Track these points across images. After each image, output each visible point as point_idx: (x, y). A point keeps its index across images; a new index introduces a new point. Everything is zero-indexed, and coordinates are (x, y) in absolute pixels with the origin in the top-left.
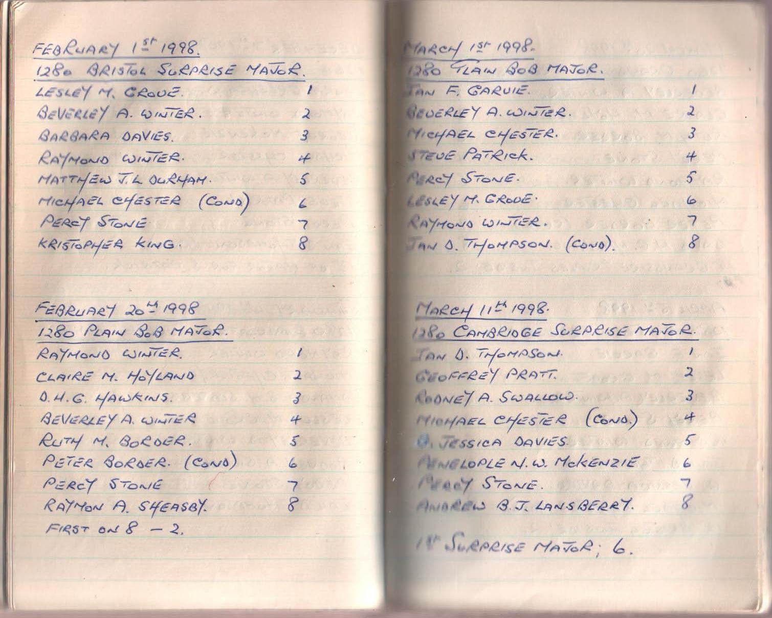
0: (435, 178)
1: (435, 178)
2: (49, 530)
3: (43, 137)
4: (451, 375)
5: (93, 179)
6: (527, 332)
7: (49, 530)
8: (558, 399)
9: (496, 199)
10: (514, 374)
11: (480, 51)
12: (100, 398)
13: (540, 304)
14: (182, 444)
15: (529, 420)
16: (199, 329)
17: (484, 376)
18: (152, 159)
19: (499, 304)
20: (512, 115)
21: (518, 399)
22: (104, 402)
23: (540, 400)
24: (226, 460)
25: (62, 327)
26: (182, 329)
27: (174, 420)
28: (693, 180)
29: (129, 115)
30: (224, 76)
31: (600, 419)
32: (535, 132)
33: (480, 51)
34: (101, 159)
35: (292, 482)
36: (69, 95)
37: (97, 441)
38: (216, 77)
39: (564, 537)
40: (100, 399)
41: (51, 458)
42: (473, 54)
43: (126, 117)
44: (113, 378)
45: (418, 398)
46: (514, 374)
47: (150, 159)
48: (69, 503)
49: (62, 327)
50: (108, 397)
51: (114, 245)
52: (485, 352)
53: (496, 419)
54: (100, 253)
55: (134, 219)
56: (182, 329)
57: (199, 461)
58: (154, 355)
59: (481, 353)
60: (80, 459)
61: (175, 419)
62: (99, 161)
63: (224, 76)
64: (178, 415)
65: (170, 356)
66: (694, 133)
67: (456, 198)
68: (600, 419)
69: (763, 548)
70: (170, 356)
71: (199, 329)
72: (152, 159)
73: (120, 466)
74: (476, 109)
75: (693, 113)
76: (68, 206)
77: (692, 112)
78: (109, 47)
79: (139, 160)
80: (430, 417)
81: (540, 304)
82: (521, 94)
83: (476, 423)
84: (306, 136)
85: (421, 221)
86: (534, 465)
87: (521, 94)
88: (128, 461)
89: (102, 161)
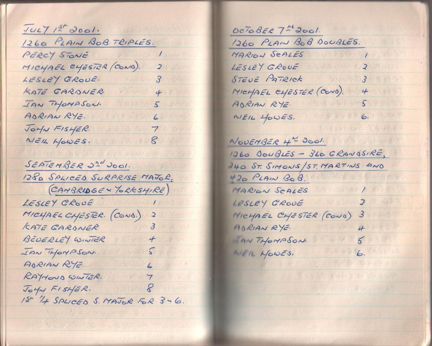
0: (43, 55)
1: (43, 55)
2: (52, 289)
4: (56, 127)
5: (76, 289)
7: (52, 289)
9: (76, 302)
10: (62, 302)
12: (42, 215)
14: (61, 217)
15: (287, 252)
16: (157, 176)
19: (289, 26)
22: (73, 292)
24: (133, 214)
26: (148, 190)
27: (37, 202)
32: (307, 214)
34: (131, 215)
35: (280, 28)
41: (267, 41)
43: (237, 106)
45: (235, 227)
46: (62, 302)
47: (83, 277)
49: (38, 174)
50: (256, 215)
51: (269, 31)
56: (148, 190)
59: (29, 103)
61: (307, 215)
62: (130, 216)
64: (44, 89)
66: (312, 42)
69: (428, 320)
71: (157, 176)
73: (290, 205)
75: (366, 68)
77: (366, 67)
80: (240, 213)
83: (267, 217)
84: (365, 80)
85: (253, 227)
88: (248, 226)
89: (131, 216)
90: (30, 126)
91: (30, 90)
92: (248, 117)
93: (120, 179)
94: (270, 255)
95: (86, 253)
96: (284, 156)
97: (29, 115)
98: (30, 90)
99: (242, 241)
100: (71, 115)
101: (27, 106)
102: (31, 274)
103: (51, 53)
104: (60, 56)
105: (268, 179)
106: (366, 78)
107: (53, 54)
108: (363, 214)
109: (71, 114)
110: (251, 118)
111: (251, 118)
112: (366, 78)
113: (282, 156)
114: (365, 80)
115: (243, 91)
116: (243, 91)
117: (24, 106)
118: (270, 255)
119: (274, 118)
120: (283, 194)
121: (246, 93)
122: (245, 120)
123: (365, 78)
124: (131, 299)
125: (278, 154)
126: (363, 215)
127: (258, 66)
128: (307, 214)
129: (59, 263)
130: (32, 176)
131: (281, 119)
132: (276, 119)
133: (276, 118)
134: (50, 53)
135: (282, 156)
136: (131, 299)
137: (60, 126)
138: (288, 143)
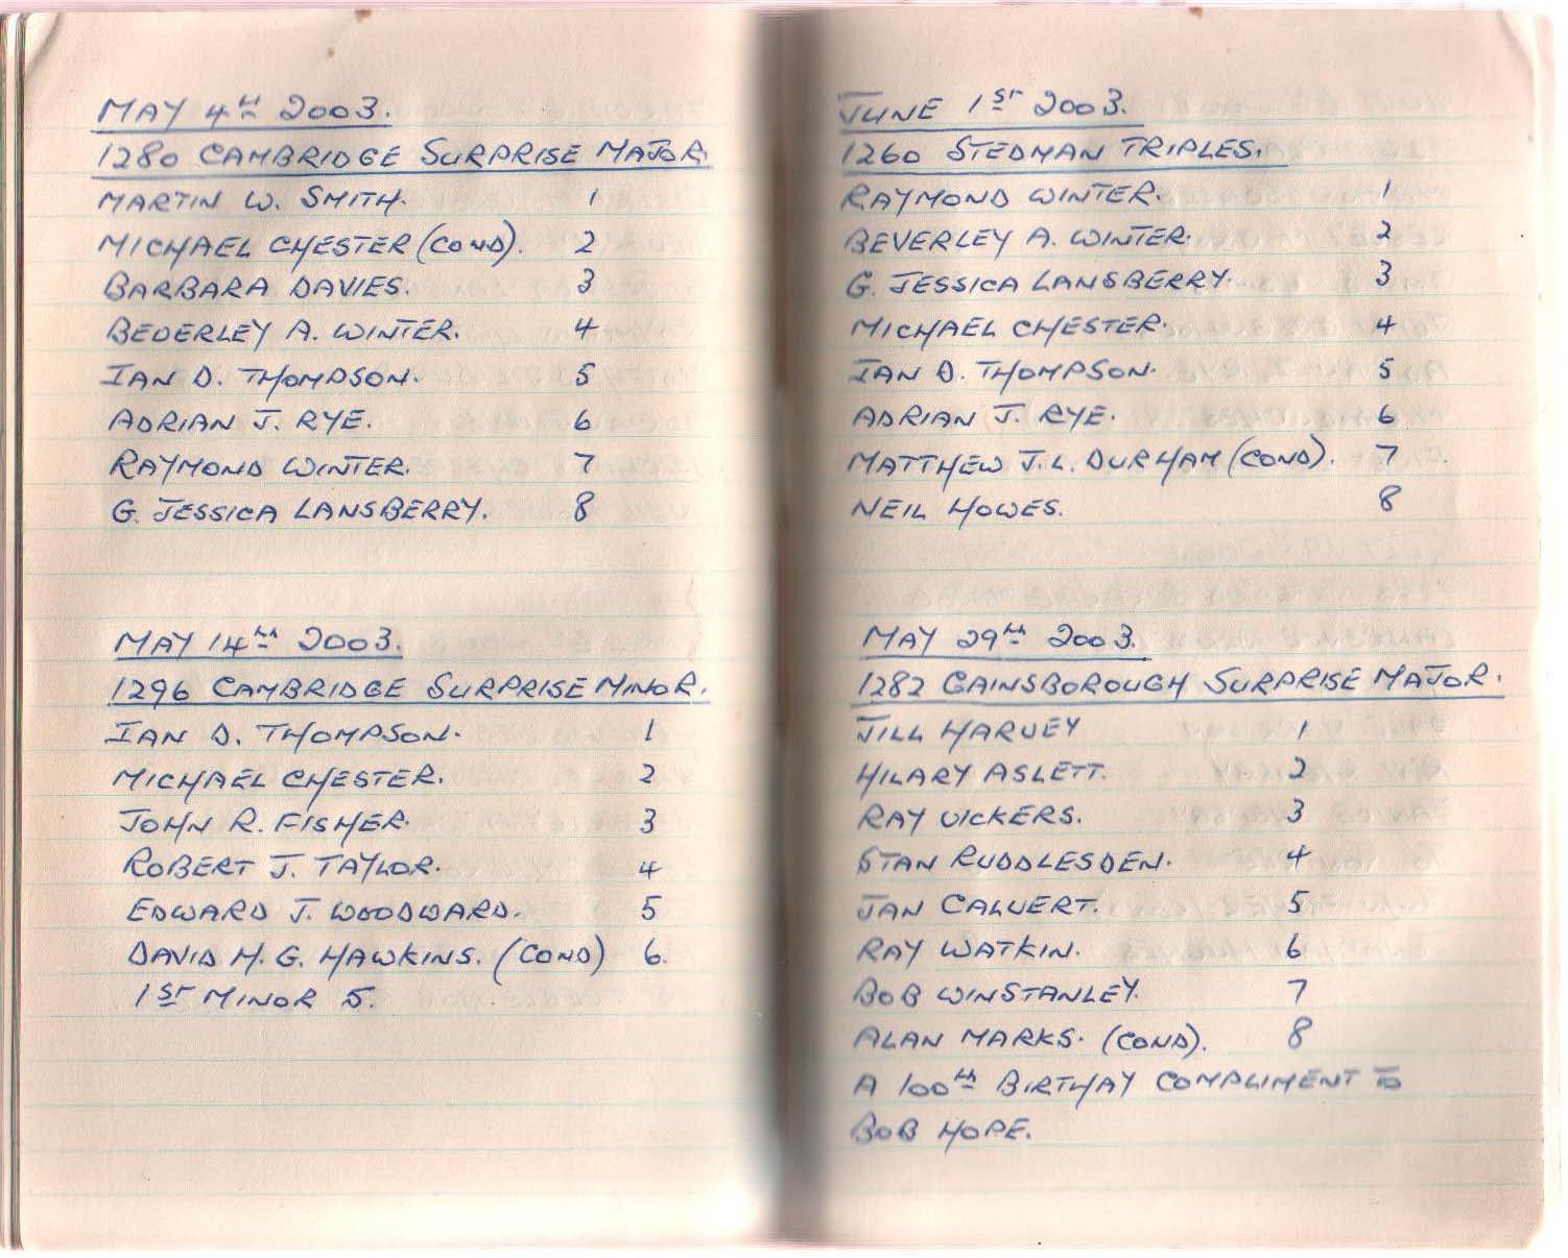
3: (114, 289)
6: (375, 689)
8: (439, 161)
11: (998, 109)
13: (581, 495)
17: (1037, 906)
18: (1135, 240)
20: (256, 208)
21: (954, 999)
23: (306, 517)
25: (157, 146)
28: (1012, 332)
29: (311, 335)
30: (559, 165)
31: (1131, 1040)
33: (998, 109)
36: (900, 739)
37: (969, 1035)
38: (1108, 120)
39: (164, 884)
40: (187, 784)
42: (986, 115)
44: (259, 958)
48: (927, 634)
52: (993, 369)
53: (288, 776)
54: (184, 838)
55: (206, 790)
57: (297, 777)
58: (1061, 199)
60: (342, 773)
63: (559, 165)
65: (413, 783)
67: (1007, 237)
68: (1131, 1040)
70: (413, 783)
72: (1135, 240)
74: (1131, 984)
76: (1164, 467)
78: (162, 108)
79: (1139, 240)
81: (581, 495)
82: (994, 157)
86: (333, 917)
87: (994, 157)
90: (268, 414)
91: (1004, 814)
92: (902, 507)
93: (234, 916)
94: (1025, 374)
95: (1034, 374)
96: (1002, 859)
97: (980, 682)
98: (1004, 814)
99: (877, 375)
100: (458, 508)
101: (115, 383)
102: (1242, 460)
103: (171, 103)
104: (297, 949)
105: (923, 777)
106: (1388, 270)
107: (932, 635)
108: (650, 821)
109: (457, 505)
110: (911, 512)
111: (911, 512)
112: (1388, 270)
113: (865, 119)
114: (1386, 274)
115: (971, 814)
116: (971, 814)
117: (106, 383)
118: (1025, 374)
119: (998, 513)
120: (946, 786)
121: (296, 782)
122: (1090, 1002)
123: (1386, 267)
124: (398, 458)
125: (292, 689)
126: (652, 826)
127: (952, 770)
128: (1149, 233)
129: (271, 857)
130: (136, 153)
131: (1022, 517)
132: (1006, 514)
133: (1006, 511)
134: (956, 768)
135: (865, 119)
136: (398, 458)
137: (185, 820)
138: (236, 648)
